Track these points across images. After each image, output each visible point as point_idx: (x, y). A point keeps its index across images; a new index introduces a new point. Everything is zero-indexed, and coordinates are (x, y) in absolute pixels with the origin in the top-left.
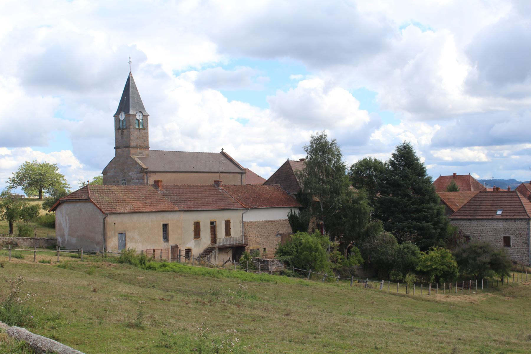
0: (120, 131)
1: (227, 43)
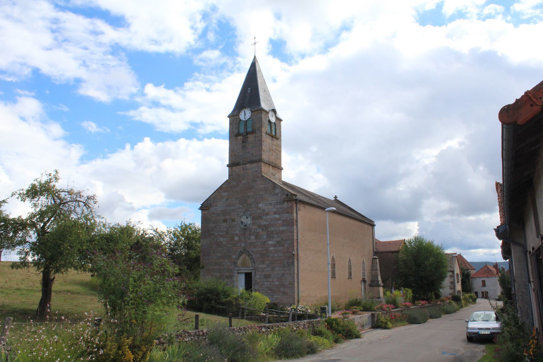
0: (240, 138)
1: (171, 193)
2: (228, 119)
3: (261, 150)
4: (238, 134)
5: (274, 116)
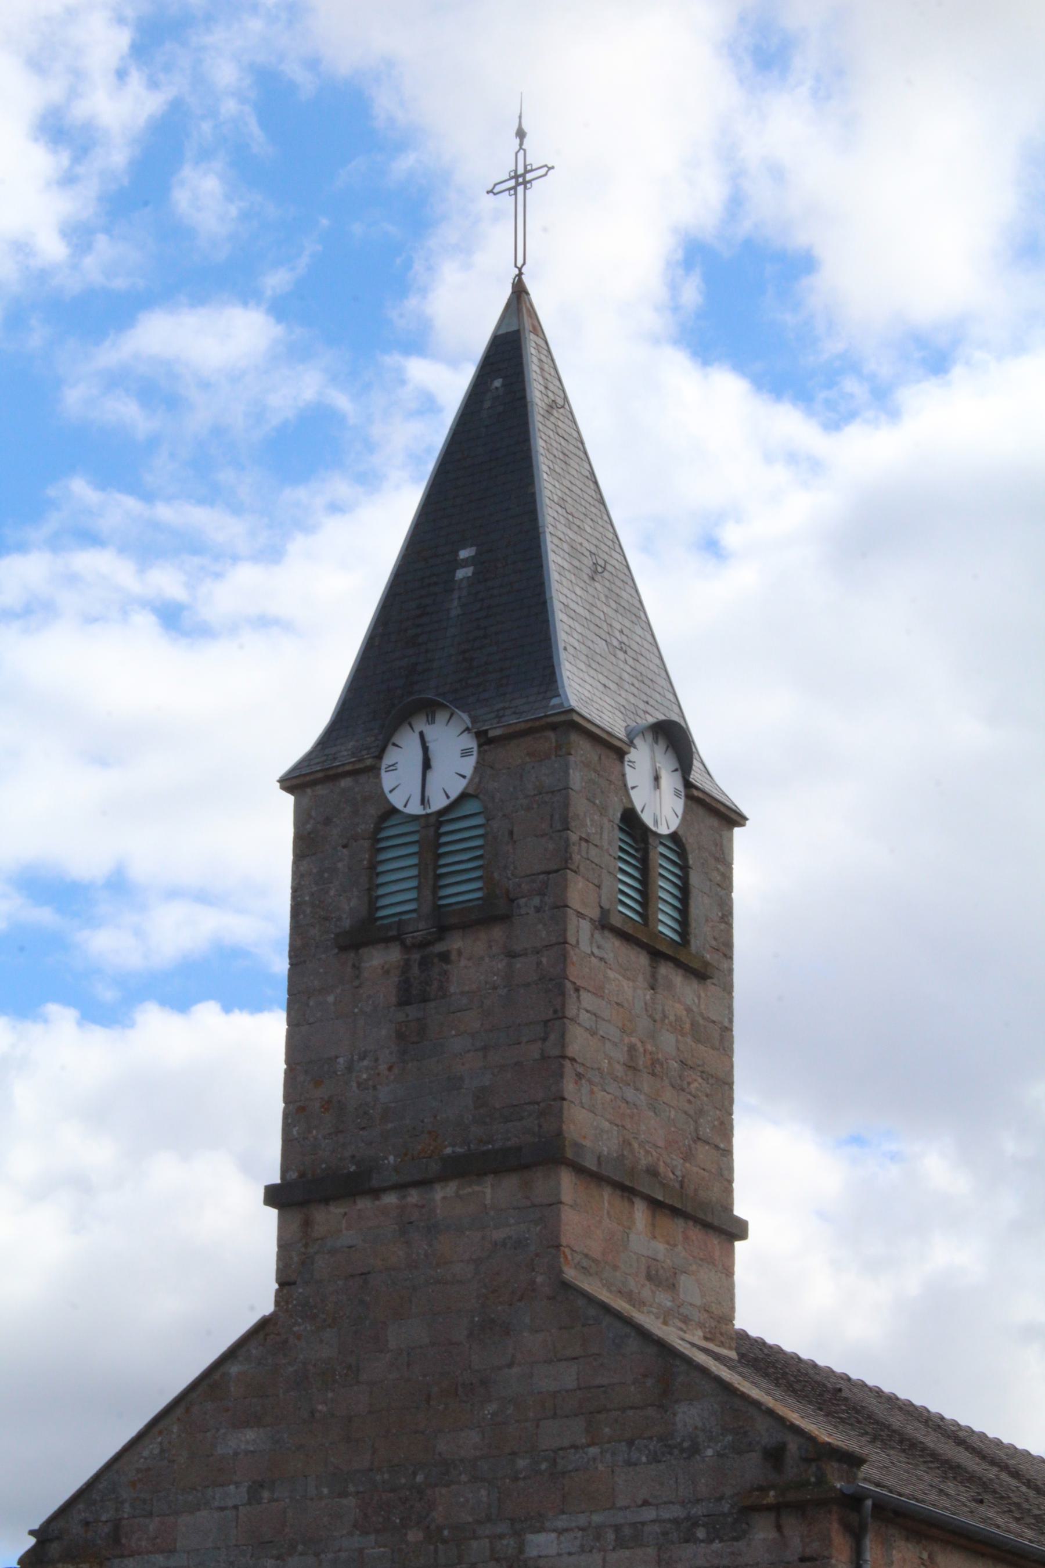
0: (380, 959)
2: (288, 800)
3: (554, 1063)
4: (364, 933)
5: (670, 781)
